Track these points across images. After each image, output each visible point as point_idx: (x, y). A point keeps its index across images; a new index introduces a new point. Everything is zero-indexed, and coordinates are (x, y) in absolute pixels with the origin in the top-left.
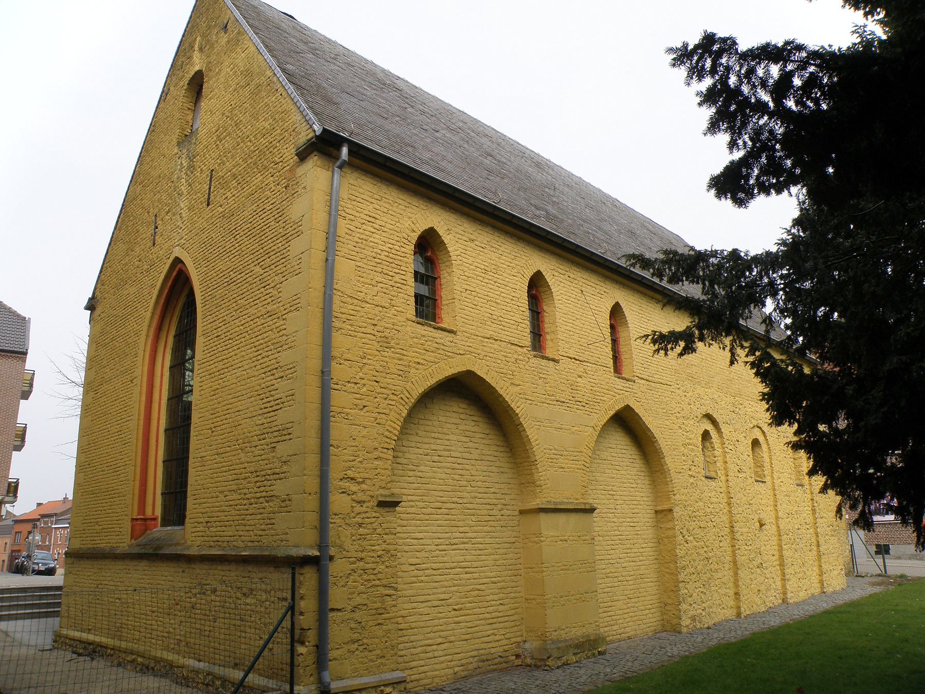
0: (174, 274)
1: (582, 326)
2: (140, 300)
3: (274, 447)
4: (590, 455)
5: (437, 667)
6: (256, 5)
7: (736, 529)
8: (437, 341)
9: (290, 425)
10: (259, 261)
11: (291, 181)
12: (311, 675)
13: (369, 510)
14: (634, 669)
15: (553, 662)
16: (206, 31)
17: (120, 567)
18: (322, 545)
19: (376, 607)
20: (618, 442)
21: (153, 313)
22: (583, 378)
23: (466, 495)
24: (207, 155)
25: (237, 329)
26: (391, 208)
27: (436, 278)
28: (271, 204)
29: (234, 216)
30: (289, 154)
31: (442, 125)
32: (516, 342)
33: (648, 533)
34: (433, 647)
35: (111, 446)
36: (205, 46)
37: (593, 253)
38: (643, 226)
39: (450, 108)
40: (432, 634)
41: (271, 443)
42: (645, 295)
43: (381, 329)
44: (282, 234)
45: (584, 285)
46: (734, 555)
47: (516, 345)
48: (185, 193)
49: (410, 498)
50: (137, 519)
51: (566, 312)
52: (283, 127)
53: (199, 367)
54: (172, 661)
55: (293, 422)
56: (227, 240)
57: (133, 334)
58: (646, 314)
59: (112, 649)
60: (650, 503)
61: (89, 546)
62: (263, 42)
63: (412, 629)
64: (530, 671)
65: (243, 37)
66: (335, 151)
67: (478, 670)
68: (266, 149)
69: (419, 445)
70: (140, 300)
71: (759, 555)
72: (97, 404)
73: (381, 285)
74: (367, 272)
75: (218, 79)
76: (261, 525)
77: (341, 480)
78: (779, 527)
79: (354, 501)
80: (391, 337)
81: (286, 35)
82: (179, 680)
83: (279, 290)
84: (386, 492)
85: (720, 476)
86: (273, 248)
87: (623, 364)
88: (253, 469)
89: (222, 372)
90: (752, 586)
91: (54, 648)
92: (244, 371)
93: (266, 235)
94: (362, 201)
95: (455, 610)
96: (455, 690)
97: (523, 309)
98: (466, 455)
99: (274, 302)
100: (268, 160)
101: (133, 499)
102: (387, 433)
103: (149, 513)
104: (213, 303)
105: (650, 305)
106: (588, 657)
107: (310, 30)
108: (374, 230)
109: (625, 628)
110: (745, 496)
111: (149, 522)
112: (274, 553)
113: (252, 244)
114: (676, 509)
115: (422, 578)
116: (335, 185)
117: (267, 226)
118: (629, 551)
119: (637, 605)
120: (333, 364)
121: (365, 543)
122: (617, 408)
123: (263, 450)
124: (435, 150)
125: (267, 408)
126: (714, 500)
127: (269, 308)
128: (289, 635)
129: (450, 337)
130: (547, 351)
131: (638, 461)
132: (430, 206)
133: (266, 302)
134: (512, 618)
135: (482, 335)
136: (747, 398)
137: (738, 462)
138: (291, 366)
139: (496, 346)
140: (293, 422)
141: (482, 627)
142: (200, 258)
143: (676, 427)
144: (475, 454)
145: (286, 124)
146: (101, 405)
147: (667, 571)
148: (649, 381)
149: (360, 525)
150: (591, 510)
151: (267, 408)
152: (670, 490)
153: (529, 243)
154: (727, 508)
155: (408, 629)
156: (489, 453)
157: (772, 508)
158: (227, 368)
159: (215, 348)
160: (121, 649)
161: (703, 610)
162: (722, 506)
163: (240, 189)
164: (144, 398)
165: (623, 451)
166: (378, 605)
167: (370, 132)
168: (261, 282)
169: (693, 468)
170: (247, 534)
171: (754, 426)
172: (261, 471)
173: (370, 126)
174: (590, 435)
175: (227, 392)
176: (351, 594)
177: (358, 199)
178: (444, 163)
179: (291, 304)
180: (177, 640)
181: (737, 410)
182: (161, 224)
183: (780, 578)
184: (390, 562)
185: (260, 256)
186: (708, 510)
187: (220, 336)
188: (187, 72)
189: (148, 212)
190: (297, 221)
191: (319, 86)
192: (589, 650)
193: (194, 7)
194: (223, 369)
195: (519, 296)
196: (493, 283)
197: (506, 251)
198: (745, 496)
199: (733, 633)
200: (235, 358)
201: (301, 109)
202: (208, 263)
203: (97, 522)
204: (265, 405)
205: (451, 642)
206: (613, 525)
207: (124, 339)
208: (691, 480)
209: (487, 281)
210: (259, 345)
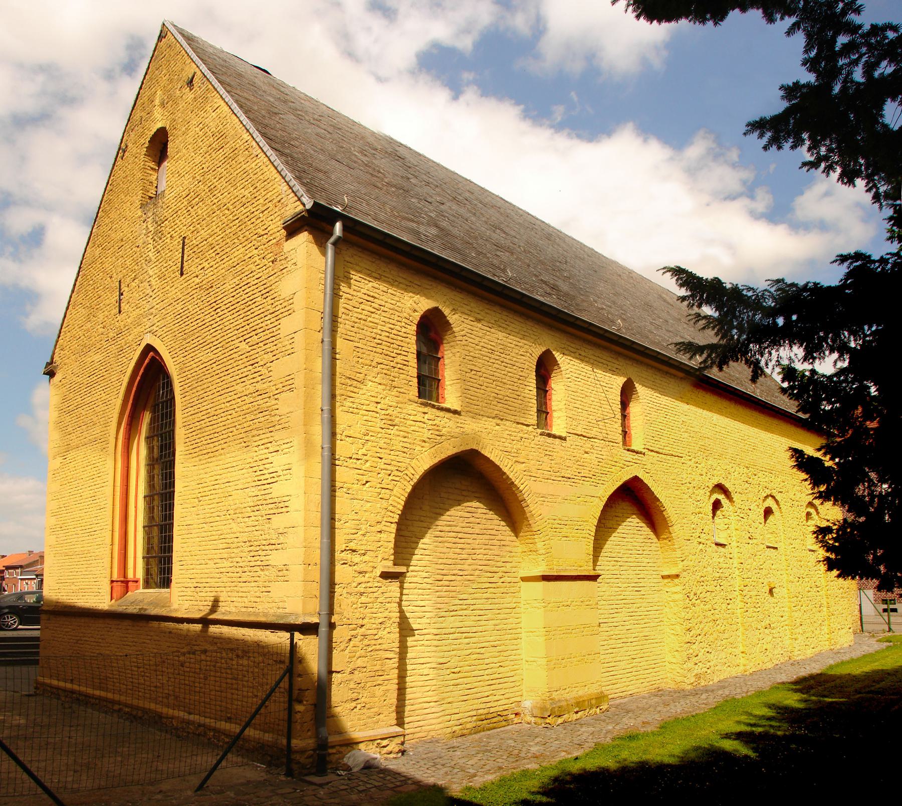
1: (591, 403)
10: (245, 337)
11: (278, 255)
13: (371, 580)
23: (465, 567)
24: (177, 221)
25: (223, 406)
29: (213, 289)
30: (276, 227)
37: (606, 331)
38: (660, 297)
44: (271, 311)
51: (574, 390)
52: (266, 197)
57: (101, 403)
62: (237, 101)
68: (247, 219)
77: (342, 551)
83: (269, 369)
86: (260, 325)
93: (252, 311)
100: (250, 231)
102: (390, 508)
103: (130, 575)
104: (194, 395)
105: (664, 380)
108: (374, 310)
127: (259, 386)
133: (255, 380)
145: (270, 194)
149: (362, 594)
153: (539, 322)
163: (218, 260)
179: (284, 385)
185: (245, 332)
189: (111, 277)
190: (287, 299)
196: (500, 363)
202: (186, 353)
204: (259, 478)
207: (91, 407)
209: (494, 361)
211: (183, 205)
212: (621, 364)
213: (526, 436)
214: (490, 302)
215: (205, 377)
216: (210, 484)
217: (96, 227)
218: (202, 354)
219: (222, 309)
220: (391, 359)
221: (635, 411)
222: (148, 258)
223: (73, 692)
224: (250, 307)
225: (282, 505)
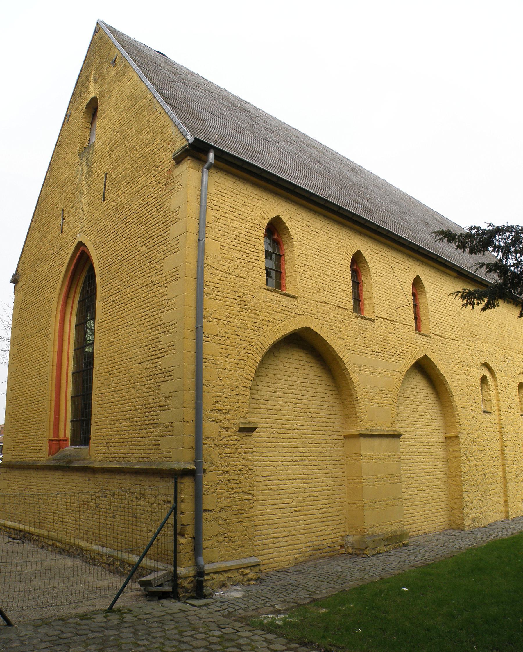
0: (78, 254)
2: (52, 275)
3: (159, 386)
4: (398, 393)
5: (283, 554)
6: (137, 45)
7: (506, 452)
8: (283, 304)
9: (171, 369)
10: (145, 242)
12: (190, 559)
13: (232, 434)
14: (432, 558)
15: (370, 551)
16: (99, 66)
17: (41, 476)
18: (197, 461)
19: (237, 509)
20: (418, 384)
21: (62, 285)
23: (303, 423)
24: (102, 162)
26: (246, 200)
28: (154, 198)
29: (124, 209)
30: (168, 158)
31: (281, 138)
33: (440, 454)
34: (279, 539)
35: (33, 385)
36: (99, 78)
38: (433, 217)
39: (285, 125)
41: (157, 383)
42: (439, 270)
43: (241, 294)
44: (163, 221)
45: (393, 262)
46: (504, 472)
47: (342, 308)
48: (85, 192)
49: (262, 425)
50: (53, 440)
53: (99, 325)
54: (83, 547)
55: (174, 366)
57: (47, 301)
58: (439, 285)
59: (37, 536)
60: (441, 431)
62: (144, 73)
63: (264, 525)
64: (352, 558)
65: (129, 69)
66: (205, 156)
67: (313, 557)
68: (148, 156)
69: (269, 384)
70: (52, 275)
72: (20, 354)
75: (110, 103)
76: (149, 445)
77: (211, 411)
79: (221, 427)
80: (248, 301)
81: (160, 68)
82: (88, 560)
83: (162, 264)
84: (245, 421)
87: (422, 323)
89: (117, 328)
90: (518, 496)
92: (134, 327)
93: (150, 222)
94: (224, 195)
95: (296, 511)
96: (296, 571)
97: (348, 280)
98: (304, 393)
99: (158, 274)
101: (50, 425)
102: (246, 375)
104: (109, 276)
105: (443, 278)
106: (396, 548)
107: (178, 65)
108: (235, 218)
110: (513, 426)
111: (62, 443)
112: (160, 467)
113: (139, 229)
114: (462, 436)
115: (271, 487)
116: (204, 183)
117: (151, 215)
118: (425, 467)
119: (431, 509)
120: (205, 321)
121: (230, 459)
122: (418, 358)
123: (150, 388)
124: (278, 156)
125: (153, 355)
126: (490, 429)
127: (154, 278)
128: (172, 529)
129: (292, 301)
130: (365, 313)
131: (433, 399)
132: (276, 199)
133: (151, 274)
134: (338, 518)
135: (317, 300)
136: (515, 351)
137: (508, 400)
138: (172, 323)
139: (327, 309)
140: (174, 366)
142: (99, 241)
143: (461, 373)
144: (311, 392)
146: (24, 354)
147: (455, 483)
149: (226, 446)
151: (153, 355)
152: (457, 421)
153: (351, 229)
154: (499, 436)
155: (261, 525)
156: (321, 391)
158: (121, 325)
159: (111, 310)
160: (49, 538)
161: (480, 513)
162: (495, 434)
163: (128, 187)
164: (56, 349)
165: (421, 391)
167: (229, 142)
168: (147, 258)
169: (474, 405)
170: (138, 452)
171: (520, 373)
172: (148, 404)
173: (228, 137)
174: (397, 378)
175: (122, 344)
176: (219, 498)
177: (222, 194)
178: (285, 167)
179: (171, 275)
180: (86, 530)
181: (508, 360)
182: (67, 216)
184: (248, 474)
185: (145, 239)
186: (485, 437)
187: (115, 301)
188: (85, 99)
189: (57, 208)
190: (175, 211)
191: (188, 107)
192: (396, 543)
193: (89, 48)
195: (344, 270)
196: (324, 259)
197: (334, 235)
198: (513, 426)
199: (505, 532)
200: (127, 317)
201: (177, 124)
202: (105, 245)
203: (23, 442)
204: (152, 354)
205: (293, 535)
208: (473, 414)
209: (320, 258)
210: (146, 308)
211: (106, 150)
212: (411, 264)
213: (346, 317)
214: (316, 213)
215: (117, 275)
216: (117, 360)
217: (49, 172)
218: (115, 245)
219: (130, 223)
220: (247, 255)
221: (423, 301)
224: (149, 220)
225: (168, 374)
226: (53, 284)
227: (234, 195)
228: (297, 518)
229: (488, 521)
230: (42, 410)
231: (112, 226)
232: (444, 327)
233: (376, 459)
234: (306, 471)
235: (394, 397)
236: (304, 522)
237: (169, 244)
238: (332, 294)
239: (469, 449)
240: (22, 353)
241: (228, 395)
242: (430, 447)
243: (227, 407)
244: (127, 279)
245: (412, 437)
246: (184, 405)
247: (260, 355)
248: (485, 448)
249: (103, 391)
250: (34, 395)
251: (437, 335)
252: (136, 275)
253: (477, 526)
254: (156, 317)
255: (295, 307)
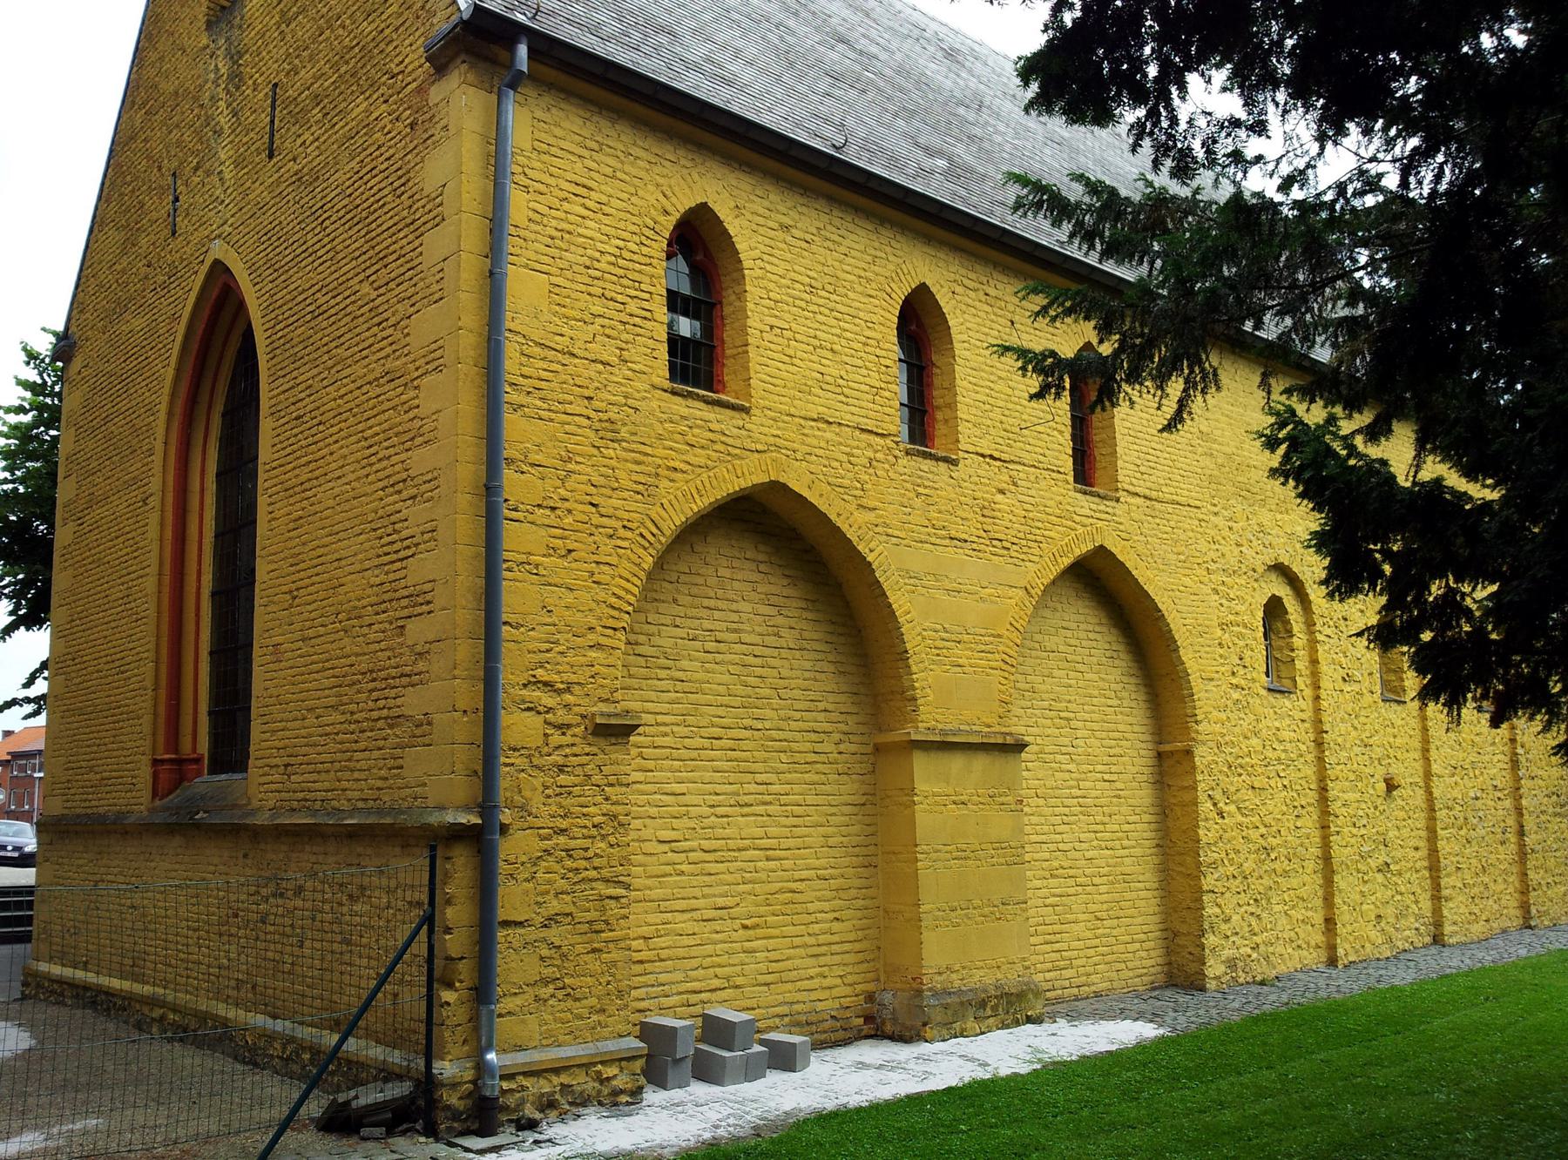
1: (1010, 392)
7: (1332, 794)
8: (712, 426)
9: (428, 587)
10: (369, 272)
13: (577, 740)
18: (487, 807)
21: (178, 370)
22: (1008, 494)
23: (769, 713)
27: (713, 305)
30: (414, 56)
32: (870, 425)
35: (113, 624)
40: (701, 971)
43: (602, 405)
44: (408, 221)
46: (1326, 845)
47: (870, 432)
48: (227, 131)
50: (163, 761)
53: (266, 476)
56: (308, 229)
60: (1143, 737)
61: (78, 811)
68: (372, 45)
71: (1382, 847)
73: (599, 321)
74: (573, 296)
77: (525, 686)
78: (1431, 793)
79: (550, 724)
80: (622, 420)
85: (1303, 687)
86: (392, 249)
87: (1098, 465)
88: (364, 667)
89: (307, 485)
90: (1365, 907)
91: (24, 997)
94: (560, 153)
95: (745, 927)
100: (378, 68)
102: (613, 600)
104: (288, 354)
109: (1088, 975)
110: (1356, 728)
113: (354, 238)
114: (1200, 751)
117: (381, 203)
118: (1100, 827)
119: (1115, 932)
122: (1077, 552)
126: (1286, 735)
129: (738, 419)
133: (383, 354)
135: (803, 413)
138: (429, 476)
139: (828, 435)
140: (434, 581)
141: (797, 962)
142: (261, 263)
148: (1150, 499)
149: (561, 769)
150: (1019, 747)
157: (1417, 755)
159: (293, 440)
161: (1253, 948)
162: (1303, 748)
165: (1091, 636)
166: (593, 915)
168: (373, 314)
169: (1242, 671)
172: (380, 670)
174: (1015, 604)
176: (543, 894)
177: (553, 150)
179: (427, 359)
182: (184, 192)
183: (1429, 894)
186: (1270, 754)
189: (160, 168)
190: (433, 195)
194: (310, 480)
195: (879, 336)
196: (827, 312)
197: (856, 246)
198: (1356, 728)
204: (386, 549)
205: (737, 987)
206: (1067, 776)
207: (128, 419)
208: (1236, 695)
209: (815, 308)
210: (372, 437)
211: (273, 21)
213: (880, 456)
214: (806, 191)
218: (301, 274)
219: (333, 219)
222: (218, 128)
223: (86, 987)
226: (156, 369)
227: (586, 153)
228: (747, 944)
229: (1275, 968)
230: (137, 686)
231: (291, 225)
232: (1159, 474)
233: (955, 803)
234: (773, 831)
235: (1008, 650)
236: (768, 954)
237: (422, 279)
238: (844, 399)
239: (1222, 785)
240: (85, 542)
241: (568, 648)
242: (1114, 777)
243: (565, 677)
244: (330, 363)
245: (1064, 750)
246: (456, 672)
247: (651, 551)
248: (1272, 783)
249: (280, 639)
250: (117, 649)
251: (1137, 494)
252: (349, 353)
253: (1241, 980)
254: (395, 459)
255: (744, 432)
